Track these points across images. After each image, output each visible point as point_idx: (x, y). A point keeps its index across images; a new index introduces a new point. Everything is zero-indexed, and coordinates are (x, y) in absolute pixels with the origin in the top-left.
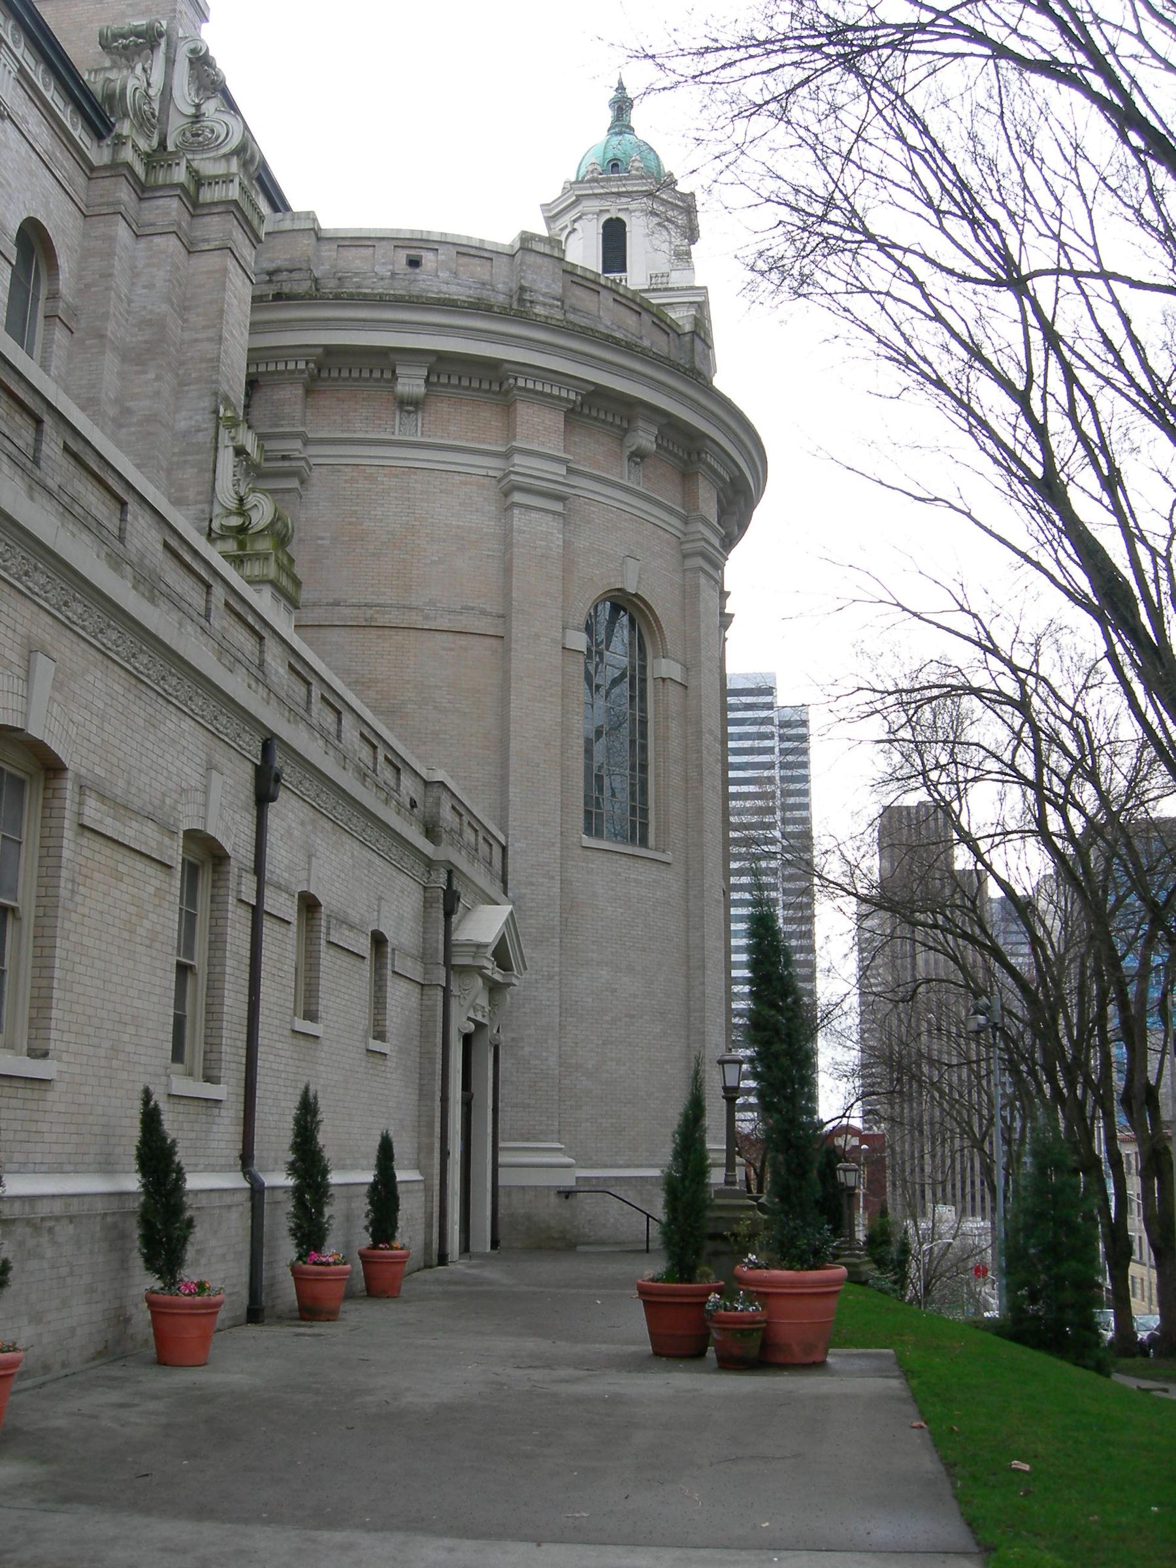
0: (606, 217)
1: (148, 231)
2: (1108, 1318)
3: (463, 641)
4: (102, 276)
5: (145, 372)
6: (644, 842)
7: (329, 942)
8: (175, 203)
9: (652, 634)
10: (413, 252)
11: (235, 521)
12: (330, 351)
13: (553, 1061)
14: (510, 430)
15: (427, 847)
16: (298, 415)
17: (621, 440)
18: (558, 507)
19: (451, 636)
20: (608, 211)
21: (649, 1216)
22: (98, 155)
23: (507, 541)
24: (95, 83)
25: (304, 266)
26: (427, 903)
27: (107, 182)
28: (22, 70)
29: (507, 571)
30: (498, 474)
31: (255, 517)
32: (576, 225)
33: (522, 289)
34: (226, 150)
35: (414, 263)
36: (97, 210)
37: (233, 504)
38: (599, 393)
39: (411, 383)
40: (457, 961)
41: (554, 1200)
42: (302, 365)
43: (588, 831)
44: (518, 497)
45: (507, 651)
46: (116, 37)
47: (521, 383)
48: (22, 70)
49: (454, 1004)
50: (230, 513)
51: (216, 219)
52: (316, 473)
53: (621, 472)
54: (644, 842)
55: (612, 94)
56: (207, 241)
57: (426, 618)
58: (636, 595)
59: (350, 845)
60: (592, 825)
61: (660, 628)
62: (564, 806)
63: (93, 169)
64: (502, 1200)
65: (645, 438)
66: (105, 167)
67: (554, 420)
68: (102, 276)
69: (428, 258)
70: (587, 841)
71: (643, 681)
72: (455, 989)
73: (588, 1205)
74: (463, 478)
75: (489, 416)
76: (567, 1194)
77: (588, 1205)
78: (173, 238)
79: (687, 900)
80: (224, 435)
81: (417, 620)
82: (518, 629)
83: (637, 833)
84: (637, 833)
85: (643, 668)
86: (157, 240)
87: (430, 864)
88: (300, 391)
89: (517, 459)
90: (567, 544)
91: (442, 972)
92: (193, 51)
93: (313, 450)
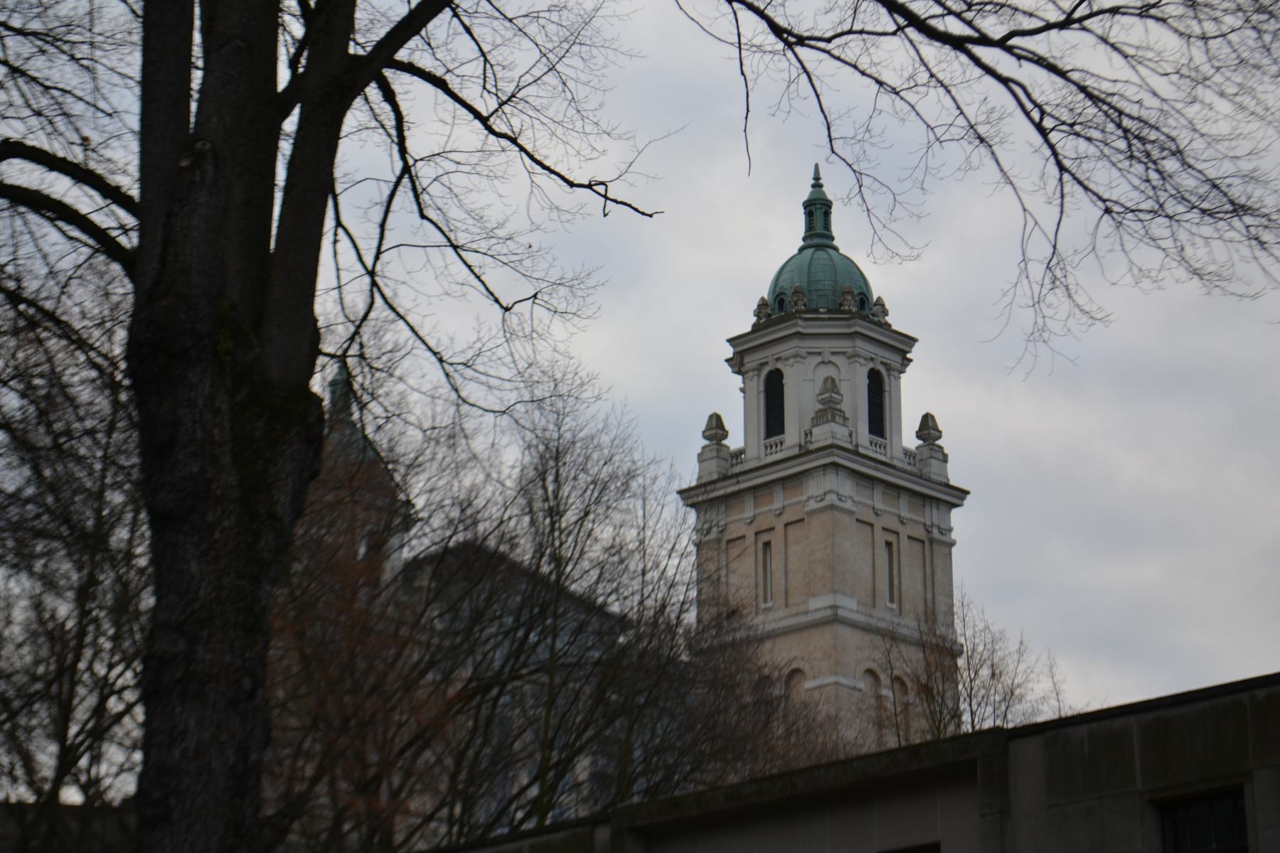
20: (820, 354)
32: (834, 359)
55: (805, 192)
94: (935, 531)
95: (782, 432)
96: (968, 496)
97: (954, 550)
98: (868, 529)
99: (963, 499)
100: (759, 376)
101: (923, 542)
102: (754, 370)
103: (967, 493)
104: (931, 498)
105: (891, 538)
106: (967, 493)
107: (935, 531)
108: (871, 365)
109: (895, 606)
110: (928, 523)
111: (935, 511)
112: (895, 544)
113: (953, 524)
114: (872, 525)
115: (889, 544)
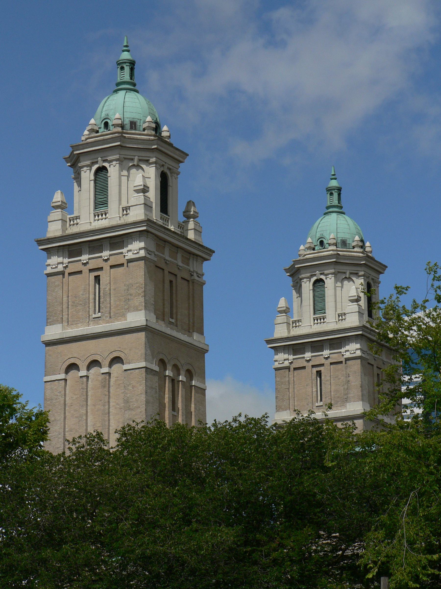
94: (195, 274)
95: (124, 70)
96: (188, 157)
97: (204, 287)
98: (161, 271)
99: (211, 256)
100: (90, 170)
101: (188, 281)
102: (87, 166)
103: (187, 155)
104: (194, 254)
105: (173, 278)
106: (187, 155)
107: (195, 274)
108: (162, 169)
109: (173, 321)
110: (192, 270)
111: (195, 262)
112: (174, 282)
113: (204, 271)
114: (163, 270)
115: (171, 282)
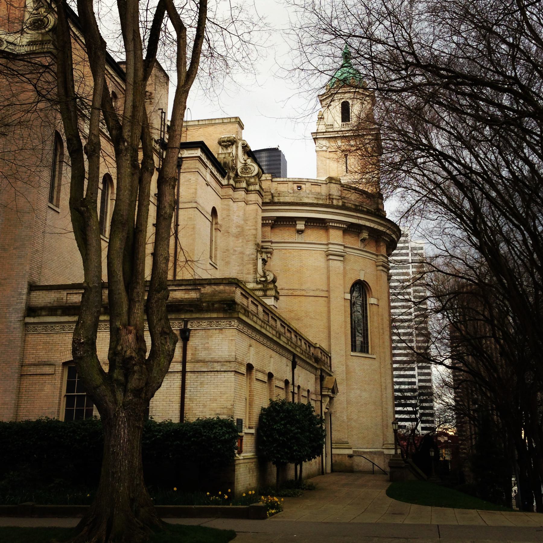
0: (343, 100)
1: (237, 200)
2: (173, 316)
3: (317, 298)
4: (227, 216)
5: (238, 240)
6: (368, 352)
7: (257, 379)
8: (243, 193)
9: (368, 291)
10: (299, 185)
11: (263, 279)
12: (278, 217)
13: (345, 418)
14: (328, 238)
15: (315, 365)
16: (269, 235)
17: (358, 236)
18: (342, 259)
19: (314, 298)
21: (373, 464)
22: (224, 182)
23: (328, 267)
24: (221, 158)
25: (269, 191)
26: (316, 379)
27: (226, 189)
28: (211, 172)
29: (328, 278)
30: (325, 250)
31: (268, 278)
33: (330, 195)
34: (253, 174)
35: (300, 188)
36: (224, 197)
37: (262, 274)
38: (352, 225)
39: (300, 226)
40: (323, 393)
41: (347, 458)
42: (270, 222)
43: (352, 351)
44: (331, 257)
45: (329, 302)
46: (224, 142)
47: (331, 224)
48: (211, 172)
49: (323, 404)
50: (262, 277)
51: (253, 195)
52: (275, 251)
53: (359, 245)
54: (368, 352)
56: (251, 201)
57: (307, 292)
58: (364, 281)
59: (304, 370)
60: (354, 349)
61: (370, 289)
62: (346, 343)
63: (222, 185)
64: (333, 458)
65: (365, 235)
66: (226, 185)
67: (340, 233)
68: (227, 216)
69: (303, 186)
70: (352, 354)
71: (366, 304)
72: (323, 401)
73: (357, 460)
74: (315, 252)
75: (322, 233)
76: (350, 456)
77: (357, 459)
78: (243, 203)
79: (380, 369)
80: (259, 256)
81: (304, 293)
82: (332, 295)
83: (364, 348)
84: (364, 348)
85: (366, 301)
86: (239, 203)
87: (316, 369)
88: (270, 229)
89: (330, 246)
90: (344, 268)
91: (320, 397)
92: (243, 144)
93: (273, 245)
